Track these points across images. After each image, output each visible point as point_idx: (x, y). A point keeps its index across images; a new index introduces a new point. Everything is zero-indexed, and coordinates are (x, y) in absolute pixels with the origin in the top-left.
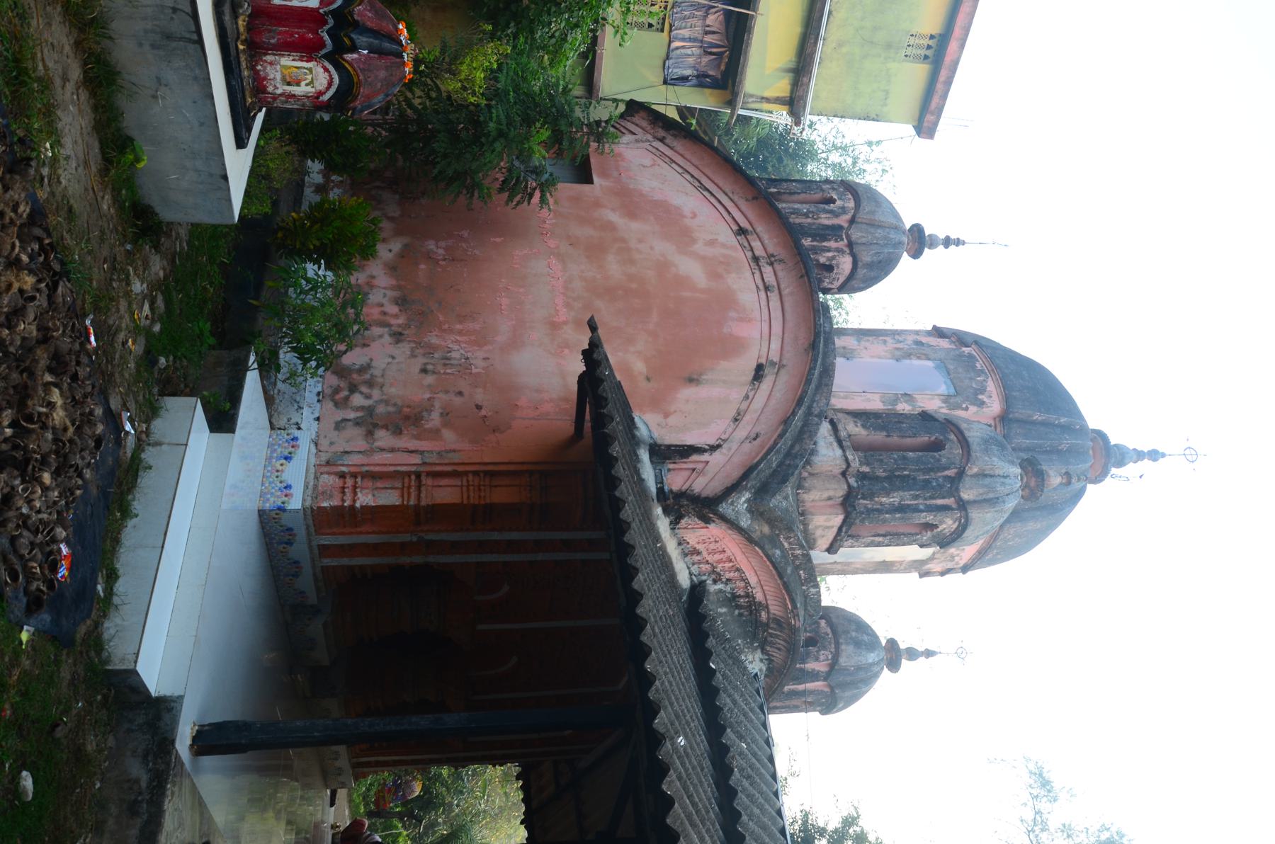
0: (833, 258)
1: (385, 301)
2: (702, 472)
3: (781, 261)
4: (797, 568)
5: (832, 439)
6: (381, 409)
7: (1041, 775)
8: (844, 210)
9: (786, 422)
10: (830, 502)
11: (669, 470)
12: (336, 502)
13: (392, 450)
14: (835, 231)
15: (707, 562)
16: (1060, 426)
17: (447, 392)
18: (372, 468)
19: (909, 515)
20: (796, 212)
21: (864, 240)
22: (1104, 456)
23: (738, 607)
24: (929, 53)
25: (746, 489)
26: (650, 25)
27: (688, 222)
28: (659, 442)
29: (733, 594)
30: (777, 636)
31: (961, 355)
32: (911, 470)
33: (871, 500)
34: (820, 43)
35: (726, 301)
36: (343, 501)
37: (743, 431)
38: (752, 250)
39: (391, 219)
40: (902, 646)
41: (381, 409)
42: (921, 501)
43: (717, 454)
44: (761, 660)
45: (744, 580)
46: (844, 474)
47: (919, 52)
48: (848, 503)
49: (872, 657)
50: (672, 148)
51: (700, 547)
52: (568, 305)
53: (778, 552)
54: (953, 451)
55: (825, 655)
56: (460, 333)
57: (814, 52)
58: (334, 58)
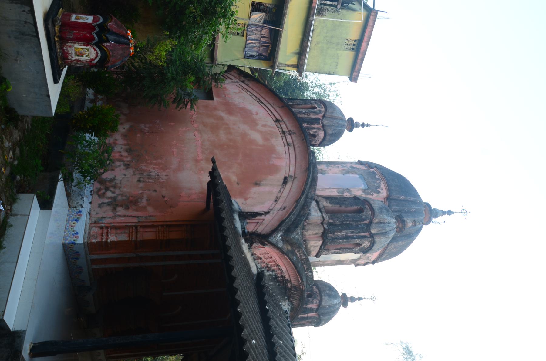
0: (316, 132)
1: (122, 150)
2: (261, 224)
3: (294, 133)
4: (303, 264)
5: (317, 208)
6: (119, 198)
7: (408, 349)
8: (320, 112)
9: (297, 201)
10: (316, 236)
11: (247, 223)
13: (125, 216)
14: (317, 121)
15: (264, 263)
16: (411, 201)
17: (149, 190)
18: (115, 224)
21: (329, 124)
22: (430, 213)
23: (278, 281)
25: (280, 230)
26: (238, 34)
27: (255, 117)
28: (243, 211)
29: (276, 276)
30: (295, 294)
31: (370, 172)
32: (350, 221)
33: (334, 234)
34: (310, 42)
35: (271, 150)
36: (102, 239)
37: (279, 206)
38: (282, 128)
39: (125, 115)
40: (348, 296)
41: (119, 198)
44: (288, 304)
45: (280, 270)
46: (322, 223)
47: (350, 47)
48: (324, 236)
49: (336, 301)
51: (261, 256)
52: (203, 152)
53: (295, 257)
55: (316, 301)
56: (155, 164)
57: (307, 46)
58: (99, 45)
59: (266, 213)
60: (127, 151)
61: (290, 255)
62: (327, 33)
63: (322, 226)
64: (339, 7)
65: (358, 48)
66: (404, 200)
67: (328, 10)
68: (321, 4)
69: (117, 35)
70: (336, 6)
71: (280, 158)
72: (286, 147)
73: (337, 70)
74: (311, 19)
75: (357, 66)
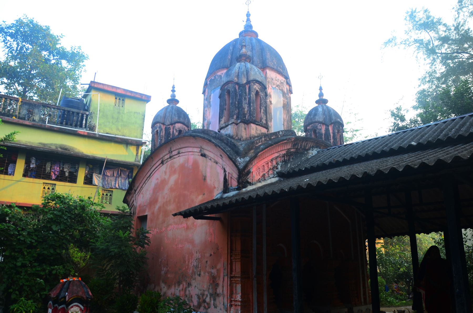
0: (176, 130)
1: (179, 289)
2: (232, 175)
3: (171, 149)
4: (270, 139)
5: (226, 129)
6: (211, 291)
7: (386, 43)
8: (160, 127)
9: (216, 145)
10: (247, 129)
11: (231, 186)
12: (239, 308)
13: (223, 287)
14: (167, 130)
15: (268, 171)
16: (233, 49)
17: (206, 267)
18: (229, 294)
19: (252, 101)
20: (160, 143)
21: (170, 120)
22: (248, 32)
23: (289, 160)
24: (121, 99)
25: (235, 159)
26: (111, 195)
27: (159, 181)
28: (222, 190)
29: (283, 162)
30: (301, 145)
31: (210, 84)
32: (236, 101)
33: (246, 114)
34: (117, 136)
35: (182, 167)
36: (239, 305)
37: (220, 161)
38: (168, 159)
39: (155, 287)
40: (318, 98)
41: (211, 291)
42: (247, 97)
43: (227, 169)
44: (312, 150)
45: (276, 158)
46: (237, 124)
47: (121, 103)
48: (247, 123)
49: (320, 109)
50: (138, 187)
51: (261, 174)
52: (182, 224)
53: (262, 147)
54: (230, 87)
55: (319, 126)
56: (189, 262)
57: (120, 138)
58: (68, 304)
59: (225, 171)
60: (179, 285)
61: (258, 150)
62: (109, 122)
63: (239, 125)
64: (87, 113)
65: (122, 96)
66: (232, 55)
67: (91, 122)
68: (85, 127)
69: (61, 290)
70: (87, 115)
71: (188, 160)
72: (181, 155)
73: (141, 113)
74: (97, 136)
75: (138, 96)
